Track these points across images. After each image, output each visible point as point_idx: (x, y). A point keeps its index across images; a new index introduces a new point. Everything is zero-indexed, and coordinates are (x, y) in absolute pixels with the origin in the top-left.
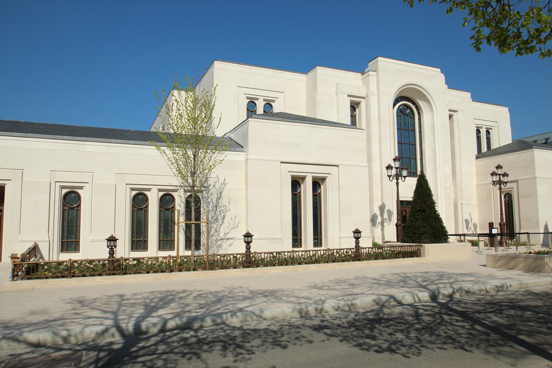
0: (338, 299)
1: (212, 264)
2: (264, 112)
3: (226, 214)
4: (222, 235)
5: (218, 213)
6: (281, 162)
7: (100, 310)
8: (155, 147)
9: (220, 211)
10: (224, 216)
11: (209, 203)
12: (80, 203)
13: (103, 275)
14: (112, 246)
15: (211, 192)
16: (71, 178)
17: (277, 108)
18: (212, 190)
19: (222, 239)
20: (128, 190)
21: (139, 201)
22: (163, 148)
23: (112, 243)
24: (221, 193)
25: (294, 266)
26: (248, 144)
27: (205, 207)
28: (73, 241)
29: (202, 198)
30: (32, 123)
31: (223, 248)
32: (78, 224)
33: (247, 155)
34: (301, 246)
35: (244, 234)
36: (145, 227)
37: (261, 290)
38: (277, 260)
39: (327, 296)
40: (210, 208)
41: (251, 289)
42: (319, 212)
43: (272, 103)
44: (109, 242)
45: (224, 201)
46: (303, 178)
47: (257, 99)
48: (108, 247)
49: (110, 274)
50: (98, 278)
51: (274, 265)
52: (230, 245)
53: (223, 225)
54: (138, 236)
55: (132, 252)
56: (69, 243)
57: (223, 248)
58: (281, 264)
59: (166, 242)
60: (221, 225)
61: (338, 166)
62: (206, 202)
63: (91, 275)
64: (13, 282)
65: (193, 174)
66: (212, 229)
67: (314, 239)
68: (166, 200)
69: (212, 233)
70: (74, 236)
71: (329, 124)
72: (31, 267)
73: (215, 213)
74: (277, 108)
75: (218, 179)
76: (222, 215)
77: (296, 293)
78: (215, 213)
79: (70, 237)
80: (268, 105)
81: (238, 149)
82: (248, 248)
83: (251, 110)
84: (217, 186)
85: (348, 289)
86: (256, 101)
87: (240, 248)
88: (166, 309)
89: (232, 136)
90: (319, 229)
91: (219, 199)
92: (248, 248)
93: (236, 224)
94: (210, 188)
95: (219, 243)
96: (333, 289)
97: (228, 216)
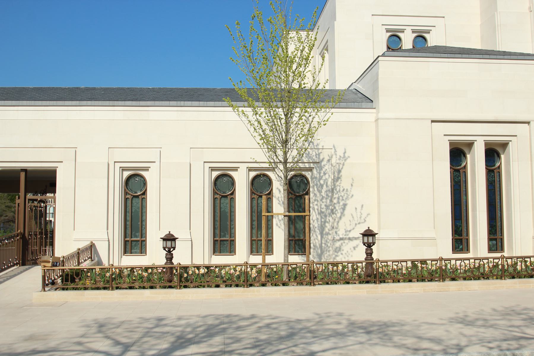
0: (491, 345)
1: (309, 277)
2: (388, 48)
3: (347, 202)
4: (341, 233)
5: (335, 201)
6: (433, 121)
7: (113, 339)
8: (231, 109)
9: (338, 198)
10: (345, 205)
11: (322, 186)
12: (146, 190)
13: (156, 288)
14: (169, 249)
15: (324, 170)
16: (134, 157)
17: (433, 40)
18: (326, 167)
19: (341, 239)
20: (207, 170)
21: (222, 186)
22: (240, 109)
23: (169, 244)
24: (339, 171)
25: (503, 281)
26: (378, 96)
27: (316, 192)
28: (139, 241)
29: (312, 178)
30: (94, 89)
31: (343, 253)
32: (144, 218)
33: (378, 113)
34: (468, 250)
35: (362, 232)
36: (231, 221)
37: (369, 321)
38: (419, 272)
39: (473, 338)
40: (323, 194)
41: (353, 318)
42: (498, 198)
43: (426, 35)
44: (165, 242)
45: (344, 183)
46: (470, 145)
47: (402, 31)
48: (164, 249)
49: (165, 287)
50: (148, 292)
51: (410, 281)
52: (354, 248)
53: (343, 219)
54: (222, 234)
55: (213, 257)
56: (134, 243)
57: (343, 253)
58: (421, 279)
59: (260, 242)
60: (340, 218)
61: (528, 123)
62: (317, 185)
63: (140, 288)
64: (43, 293)
65: (285, 142)
66: (327, 224)
67: (490, 239)
68: (260, 185)
69: (327, 230)
70: (139, 234)
71: (512, 57)
72: (70, 273)
73: (331, 201)
74: (433, 40)
75: (335, 151)
76: (341, 203)
77: (424, 331)
78: (331, 201)
79: (133, 236)
80: (420, 38)
81: (364, 105)
82: (369, 254)
83: (394, 44)
84: (334, 161)
85: (518, 327)
86: (400, 35)
87: (359, 254)
88: (202, 345)
89: (359, 86)
90: (499, 224)
91: (337, 179)
92: (369, 254)
93: (363, 217)
94: (323, 164)
95: (338, 244)
96: (491, 326)
97: (351, 204)
